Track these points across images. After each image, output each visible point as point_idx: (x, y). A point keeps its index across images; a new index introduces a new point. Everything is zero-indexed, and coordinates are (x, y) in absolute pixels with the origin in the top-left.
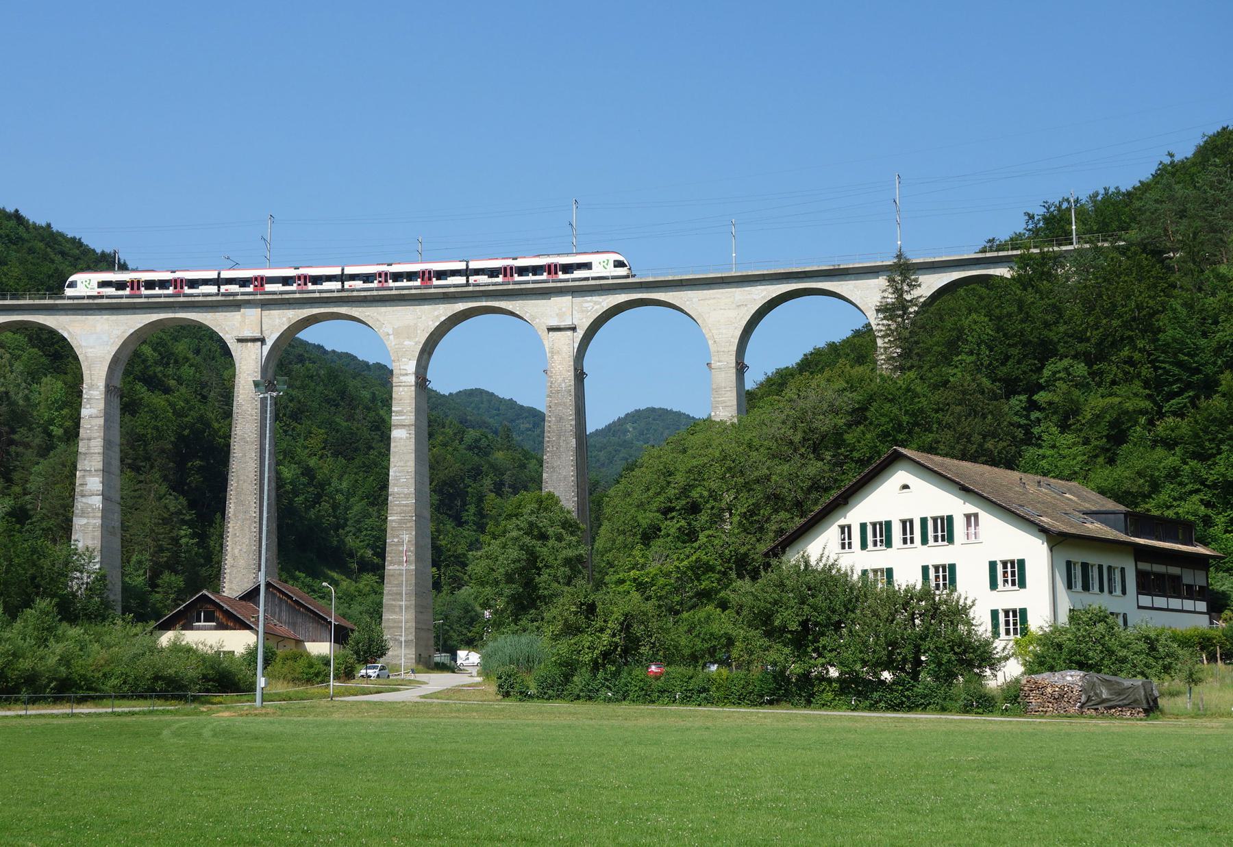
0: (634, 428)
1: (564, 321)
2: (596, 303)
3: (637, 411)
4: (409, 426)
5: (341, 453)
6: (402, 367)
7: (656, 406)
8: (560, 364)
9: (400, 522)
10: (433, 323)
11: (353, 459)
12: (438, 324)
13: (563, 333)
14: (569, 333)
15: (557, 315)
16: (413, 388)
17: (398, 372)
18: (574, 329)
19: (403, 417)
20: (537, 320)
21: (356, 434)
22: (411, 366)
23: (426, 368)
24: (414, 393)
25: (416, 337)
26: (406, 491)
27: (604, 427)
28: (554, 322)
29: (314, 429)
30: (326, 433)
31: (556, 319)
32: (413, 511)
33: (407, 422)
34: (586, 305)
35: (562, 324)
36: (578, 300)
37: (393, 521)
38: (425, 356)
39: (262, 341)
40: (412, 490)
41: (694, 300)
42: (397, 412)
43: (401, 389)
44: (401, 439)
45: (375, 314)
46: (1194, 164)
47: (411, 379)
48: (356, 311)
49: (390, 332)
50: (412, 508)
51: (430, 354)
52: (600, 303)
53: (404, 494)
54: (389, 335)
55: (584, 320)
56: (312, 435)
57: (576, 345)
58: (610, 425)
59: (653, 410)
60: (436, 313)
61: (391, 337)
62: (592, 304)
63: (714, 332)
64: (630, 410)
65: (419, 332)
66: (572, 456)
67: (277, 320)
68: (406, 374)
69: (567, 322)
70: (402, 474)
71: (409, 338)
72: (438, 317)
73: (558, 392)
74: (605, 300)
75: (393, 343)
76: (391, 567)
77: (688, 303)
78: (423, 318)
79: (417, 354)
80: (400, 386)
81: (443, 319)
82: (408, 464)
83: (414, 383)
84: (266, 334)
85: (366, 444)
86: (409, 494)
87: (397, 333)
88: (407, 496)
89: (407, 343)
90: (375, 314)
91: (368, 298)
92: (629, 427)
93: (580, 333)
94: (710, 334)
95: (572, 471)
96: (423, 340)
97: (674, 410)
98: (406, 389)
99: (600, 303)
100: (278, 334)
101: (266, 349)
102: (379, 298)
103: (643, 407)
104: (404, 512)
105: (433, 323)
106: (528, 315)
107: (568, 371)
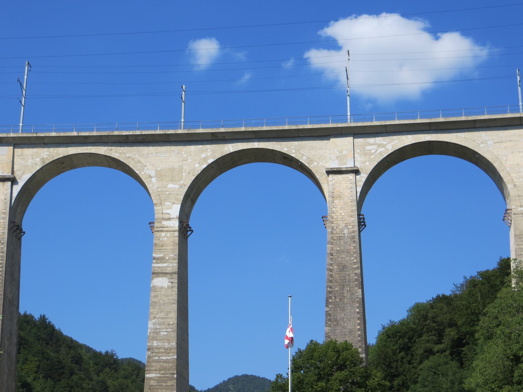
0: (234, 388)
1: (345, 164)
2: (379, 146)
3: (236, 377)
4: (171, 274)
5: (50, 377)
6: (164, 211)
7: (249, 374)
8: (341, 209)
9: (159, 380)
10: (201, 165)
11: (60, 381)
12: (205, 166)
13: (344, 176)
14: (351, 176)
15: (337, 157)
16: (177, 234)
17: (161, 216)
18: (356, 172)
19: (165, 265)
20: (315, 163)
21: (62, 362)
22: (175, 210)
23: (188, 216)
24: (177, 239)
25: (181, 180)
26: (167, 345)
27: (213, 386)
28: (335, 165)
29: (30, 357)
30: (40, 361)
31: (337, 161)
32: (175, 367)
33: (169, 270)
34: (369, 148)
35: (344, 167)
36: (359, 141)
37: (151, 379)
38: (189, 202)
39: (13, 181)
40: (174, 344)
41: (489, 143)
42: (158, 259)
43: (163, 234)
44: (162, 288)
45: (137, 156)
46: (493, 275)
47: (175, 224)
48: (116, 152)
49: (153, 174)
50: (173, 365)
51: (193, 202)
52: (384, 146)
53: (165, 349)
54: (150, 177)
55: (367, 163)
56: (28, 362)
57: (359, 189)
58: (217, 386)
59: (246, 376)
60: (203, 156)
61: (154, 180)
62: (375, 147)
63: (513, 175)
64: (232, 375)
65: (184, 174)
66: (358, 307)
67: (30, 160)
68: (169, 219)
69: (349, 165)
70: (164, 327)
71: (173, 181)
72: (205, 159)
73: (340, 238)
74: (390, 143)
75: (156, 186)
76: (361, 314)
77: (482, 145)
78: (189, 160)
79: (181, 197)
80: (162, 231)
81: (211, 161)
82: (170, 315)
83: (177, 228)
84: (17, 174)
85: (69, 370)
86: (170, 349)
87: (160, 175)
88: (167, 351)
89: (171, 186)
90: (137, 156)
91: (130, 138)
92: (231, 387)
93: (363, 178)
94: (509, 178)
95: (359, 324)
96: (188, 183)
97: (261, 377)
98: (168, 234)
99: (384, 146)
100: (31, 175)
101: (17, 189)
102: (141, 138)
103: (240, 374)
104: (165, 369)
105: (201, 165)
106: (304, 158)
107: (351, 216)
